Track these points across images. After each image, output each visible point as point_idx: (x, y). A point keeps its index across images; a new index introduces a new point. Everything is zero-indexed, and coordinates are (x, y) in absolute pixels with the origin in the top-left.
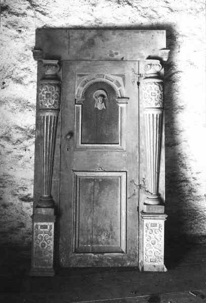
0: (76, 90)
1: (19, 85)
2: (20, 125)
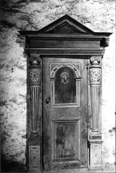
0: (51, 73)
1: (20, 70)
2: (22, 94)
